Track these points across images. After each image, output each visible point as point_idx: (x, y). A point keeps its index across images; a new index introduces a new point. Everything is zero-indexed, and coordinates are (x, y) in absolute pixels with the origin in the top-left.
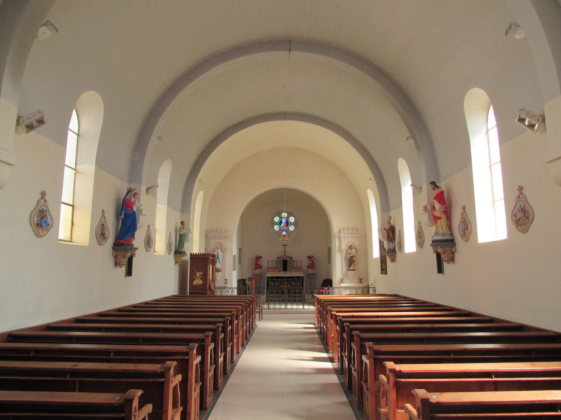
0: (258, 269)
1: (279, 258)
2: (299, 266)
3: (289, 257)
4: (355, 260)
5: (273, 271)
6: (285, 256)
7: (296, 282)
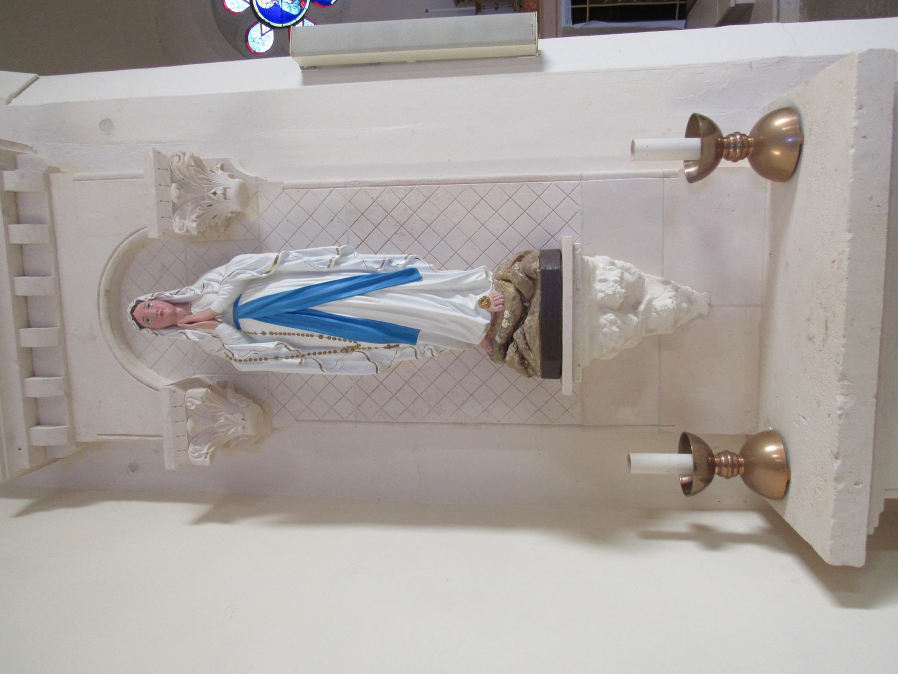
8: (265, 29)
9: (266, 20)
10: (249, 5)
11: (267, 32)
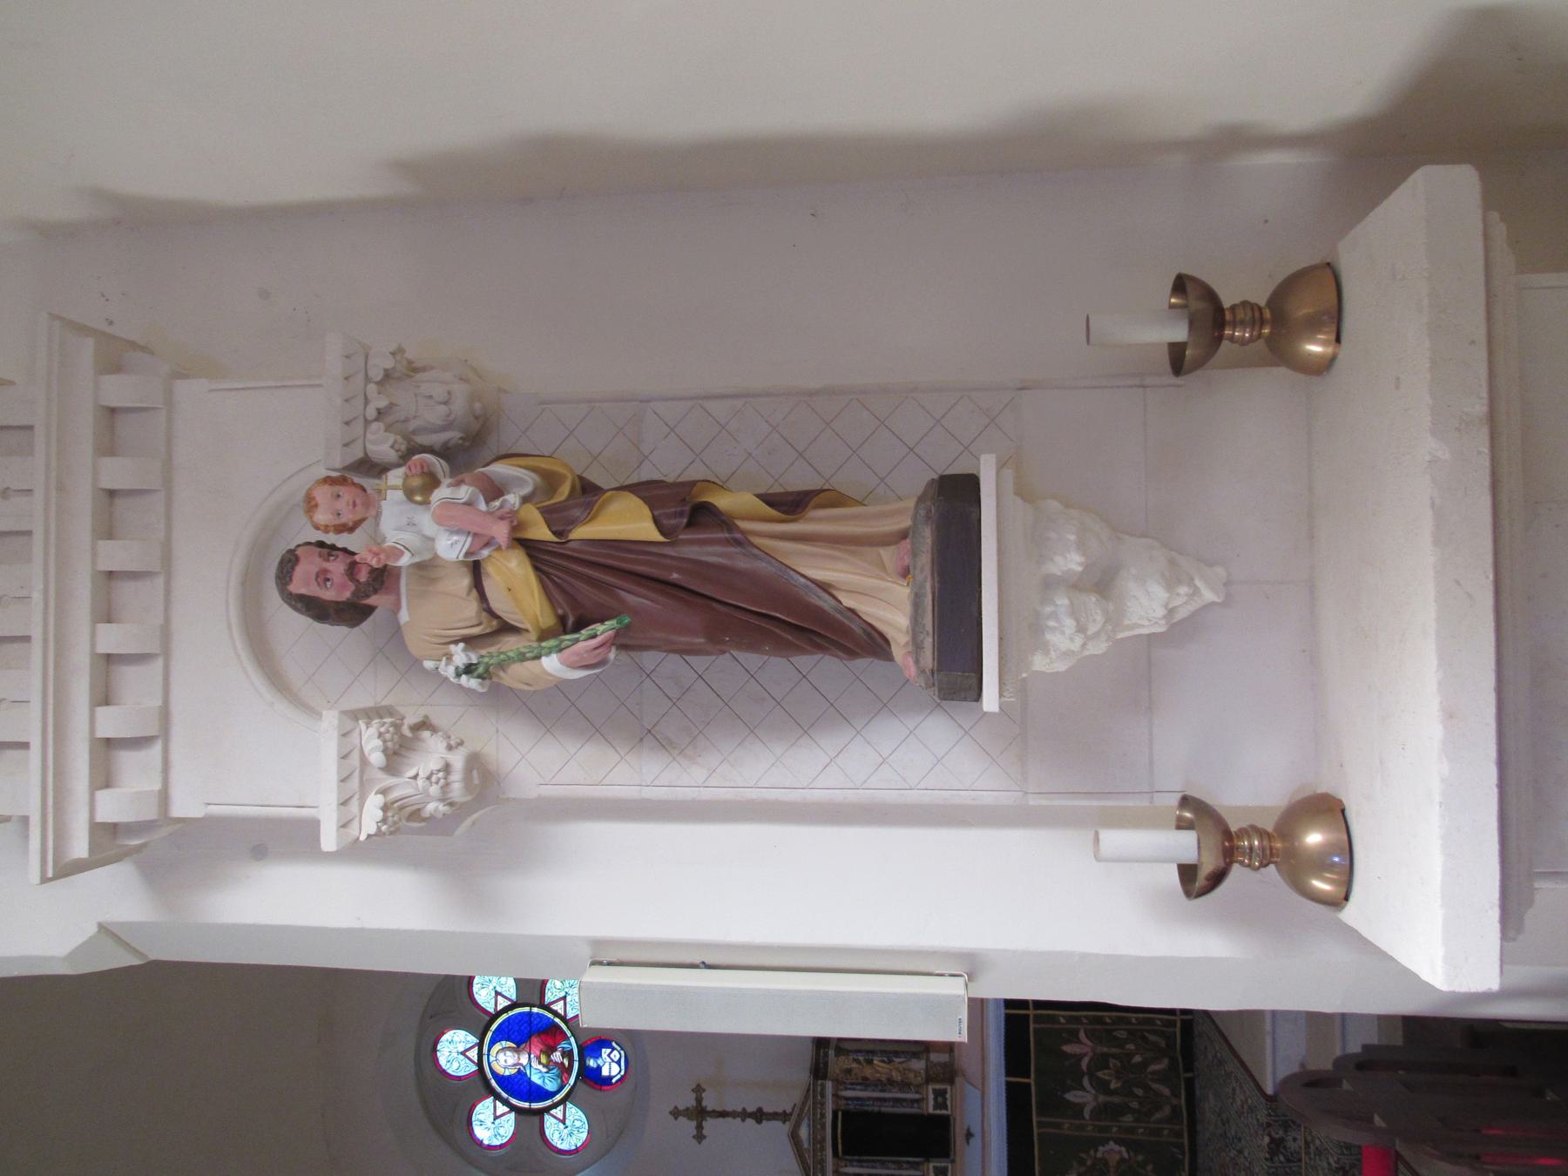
3: (813, 1095)
4: (650, 492)
9: (504, 1095)
10: (512, 1115)
11: (469, 1059)
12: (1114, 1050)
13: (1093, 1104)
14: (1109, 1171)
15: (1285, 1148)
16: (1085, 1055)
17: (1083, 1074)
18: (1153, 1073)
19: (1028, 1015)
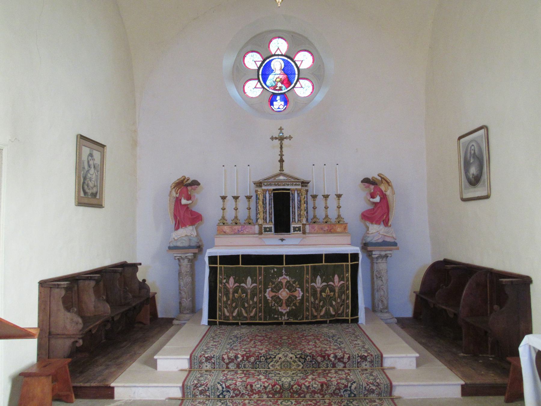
0: (184, 225)
1: (259, 184)
2: (333, 214)
5: (238, 233)
6: (282, 178)
7: (327, 278)
8: (259, 64)
12: (337, 294)
13: (316, 287)
14: (291, 292)
15: (363, 361)
16: (247, 285)
17: (327, 283)
18: (329, 309)
19: (219, 265)
